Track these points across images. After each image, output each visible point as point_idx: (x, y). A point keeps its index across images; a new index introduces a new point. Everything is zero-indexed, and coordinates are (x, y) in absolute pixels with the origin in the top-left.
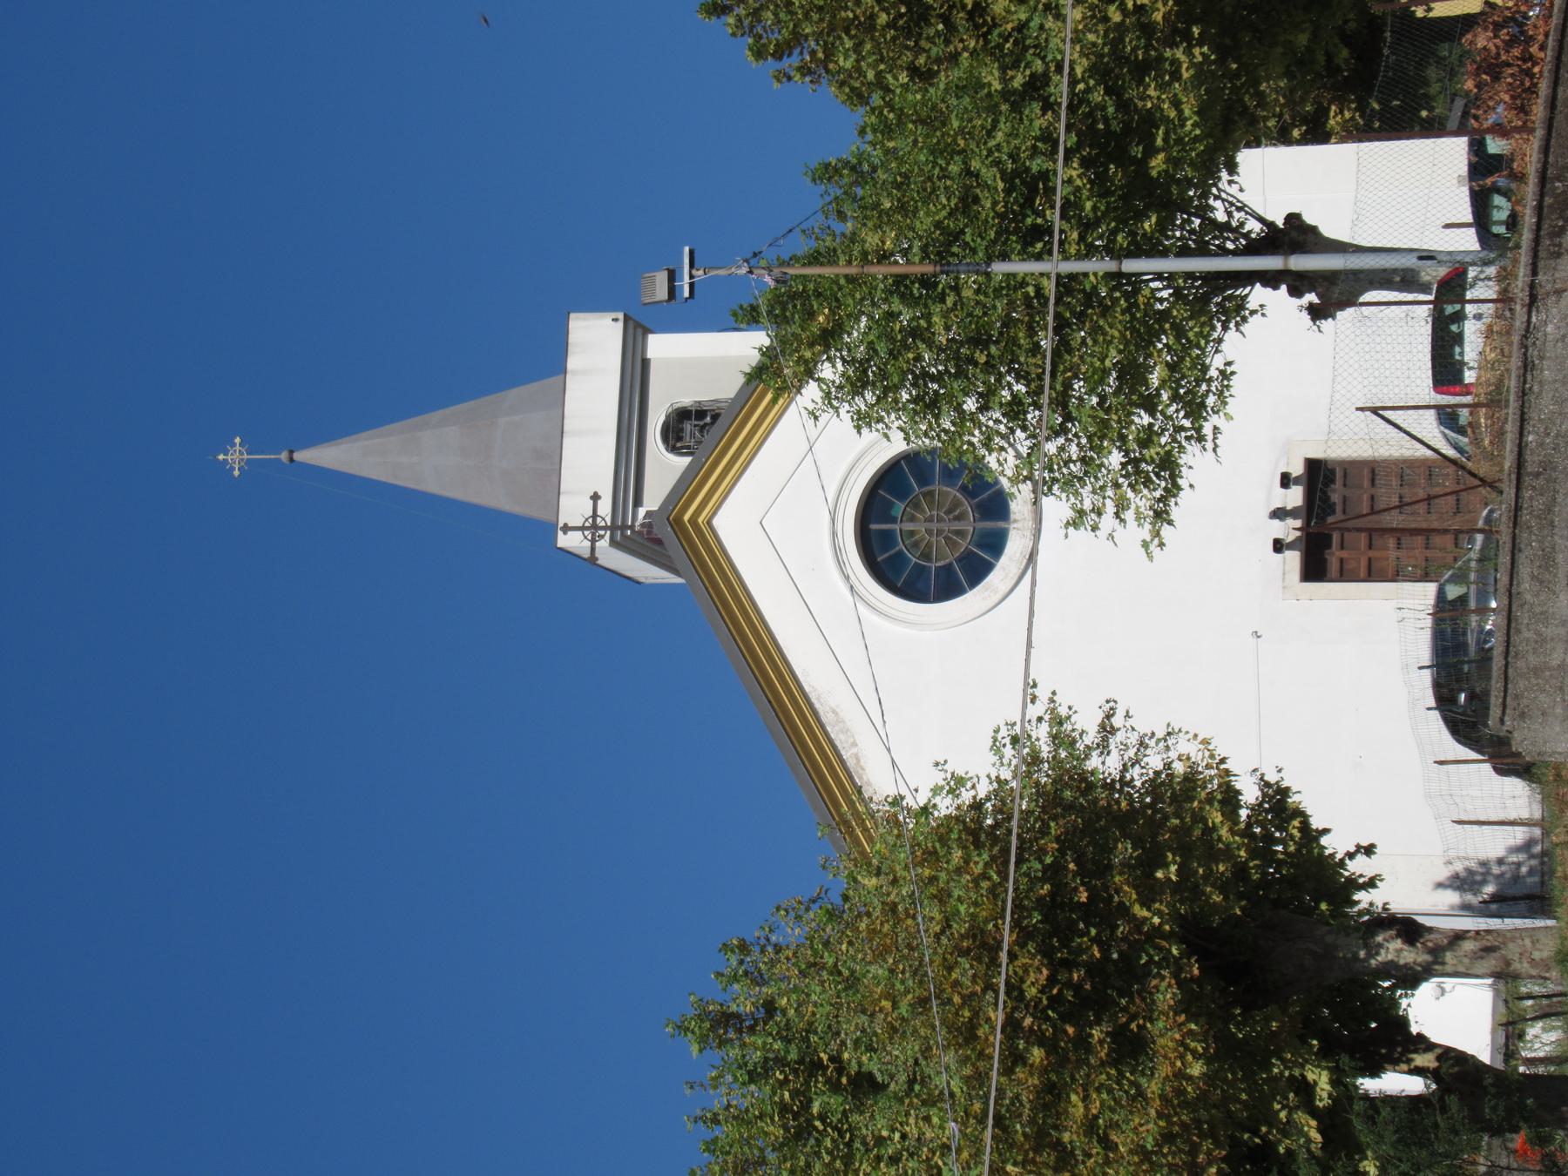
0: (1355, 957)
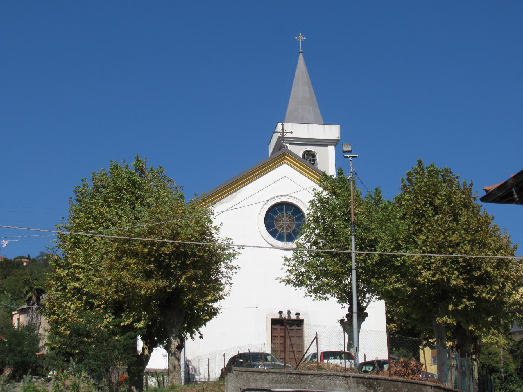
0: (173, 333)
